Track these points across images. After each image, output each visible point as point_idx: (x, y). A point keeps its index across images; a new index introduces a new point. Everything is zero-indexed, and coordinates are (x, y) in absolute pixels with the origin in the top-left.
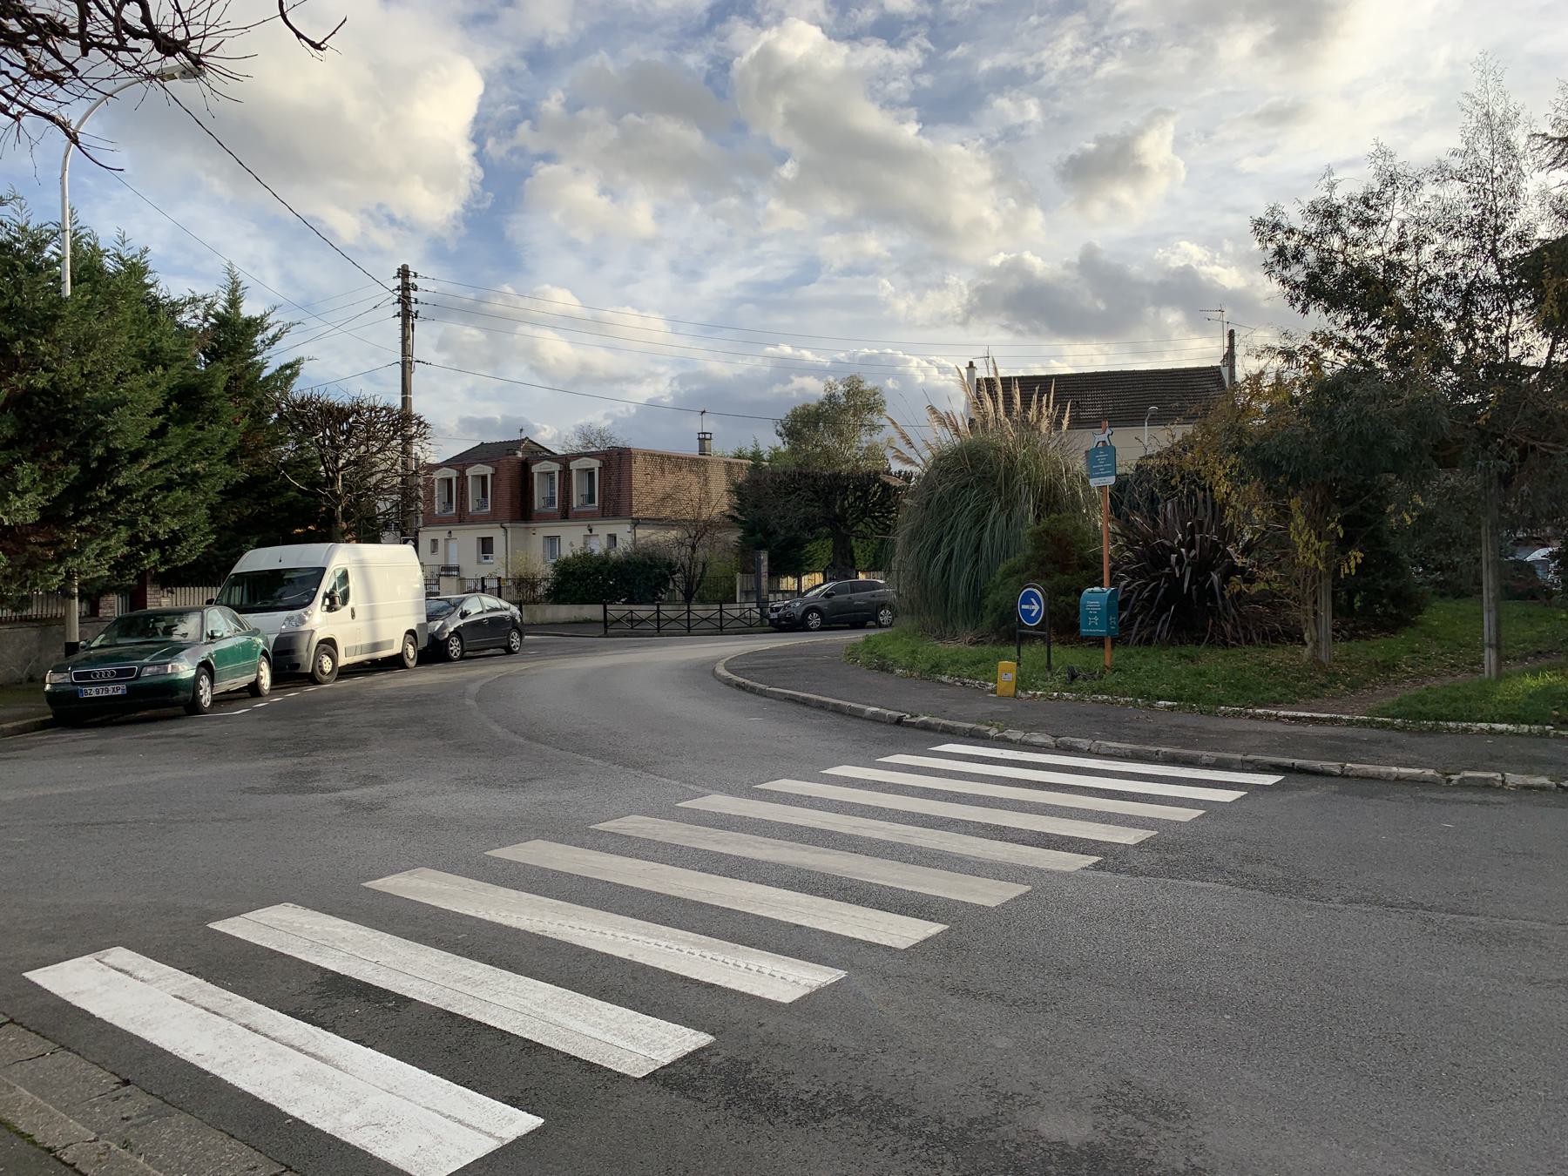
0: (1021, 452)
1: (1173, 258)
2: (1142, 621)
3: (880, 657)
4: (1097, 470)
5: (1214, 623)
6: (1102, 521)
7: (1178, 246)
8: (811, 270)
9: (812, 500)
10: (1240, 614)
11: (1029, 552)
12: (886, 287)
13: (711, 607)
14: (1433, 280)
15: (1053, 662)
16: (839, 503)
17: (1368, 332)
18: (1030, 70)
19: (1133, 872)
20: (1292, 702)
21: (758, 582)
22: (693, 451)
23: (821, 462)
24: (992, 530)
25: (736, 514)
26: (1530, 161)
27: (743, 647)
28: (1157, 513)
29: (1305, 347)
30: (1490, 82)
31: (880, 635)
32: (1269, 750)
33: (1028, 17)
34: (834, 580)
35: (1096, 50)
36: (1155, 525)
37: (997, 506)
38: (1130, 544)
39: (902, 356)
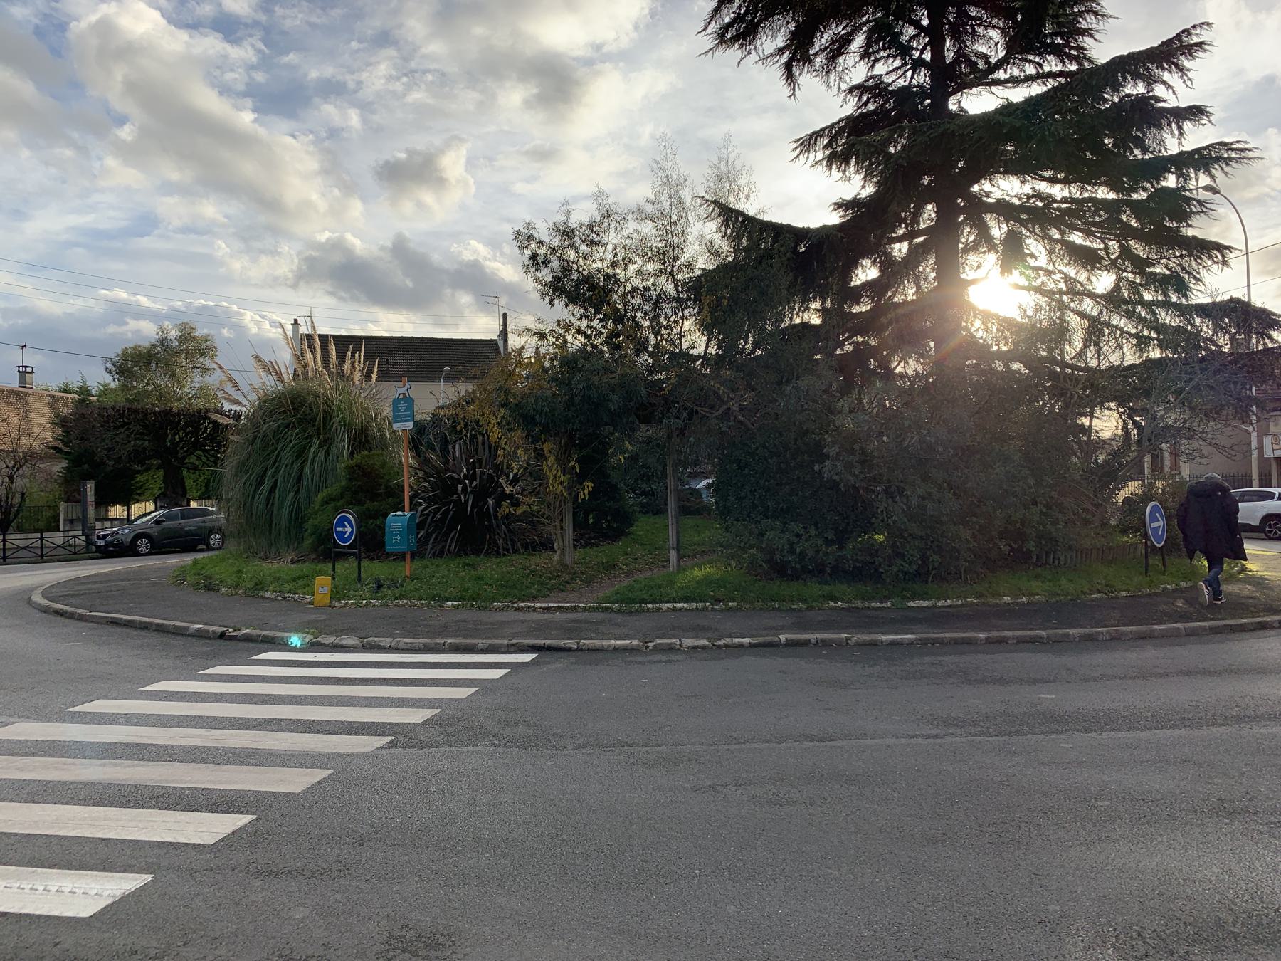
0: (337, 399)
1: (465, 252)
2: (436, 538)
3: (208, 578)
4: (399, 416)
5: (490, 537)
6: (406, 458)
7: (469, 244)
8: (146, 223)
9: (142, 434)
10: (509, 530)
11: (344, 483)
12: (222, 248)
13: (30, 536)
14: (634, 289)
15: (363, 575)
16: (170, 437)
17: (595, 323)
18: (351, 85)
19: (420, 745)
20: (546, 596)
21: (84, 511)
22: (14, 384)
23: (153, 399)
24: (312, 464)
25: (61, 446)
26: (693, 214)
27: (62, 574)
28: (448, 453)
29: (552, 330)
30: (669, 155)
31: (208, 557)
32: (527, 635)
33: (349, 43)
34: (166, 508)
35: (405, 79)
36: (447, 462)
37: (316, 443)
38: (427, 476)
39: (236, 309)
